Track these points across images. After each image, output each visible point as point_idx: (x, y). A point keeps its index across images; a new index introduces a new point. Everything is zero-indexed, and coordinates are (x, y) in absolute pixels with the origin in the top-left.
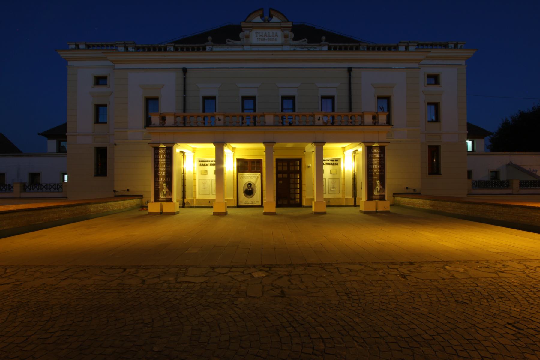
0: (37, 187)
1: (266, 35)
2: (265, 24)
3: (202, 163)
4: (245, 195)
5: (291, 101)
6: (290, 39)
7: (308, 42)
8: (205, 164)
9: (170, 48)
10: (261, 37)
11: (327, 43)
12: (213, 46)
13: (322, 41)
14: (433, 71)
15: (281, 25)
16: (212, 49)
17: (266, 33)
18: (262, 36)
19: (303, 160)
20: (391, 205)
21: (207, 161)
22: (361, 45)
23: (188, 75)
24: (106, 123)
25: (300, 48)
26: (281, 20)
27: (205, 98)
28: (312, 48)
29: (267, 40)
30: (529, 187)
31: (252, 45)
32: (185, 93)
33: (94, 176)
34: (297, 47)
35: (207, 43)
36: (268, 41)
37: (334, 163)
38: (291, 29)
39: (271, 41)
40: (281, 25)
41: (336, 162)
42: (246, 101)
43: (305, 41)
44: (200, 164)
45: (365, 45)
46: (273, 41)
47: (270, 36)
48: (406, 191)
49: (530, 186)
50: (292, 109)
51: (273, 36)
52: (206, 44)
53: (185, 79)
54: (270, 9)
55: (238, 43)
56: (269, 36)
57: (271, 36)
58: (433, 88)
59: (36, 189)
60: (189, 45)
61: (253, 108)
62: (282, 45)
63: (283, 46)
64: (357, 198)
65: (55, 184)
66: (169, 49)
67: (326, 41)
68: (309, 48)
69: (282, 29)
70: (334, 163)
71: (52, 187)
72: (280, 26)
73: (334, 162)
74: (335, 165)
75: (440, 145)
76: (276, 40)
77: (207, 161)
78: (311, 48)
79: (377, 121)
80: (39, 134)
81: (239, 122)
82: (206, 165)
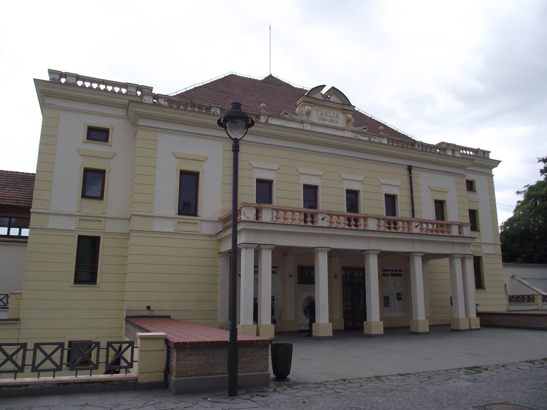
1: (327, 115)
4: (305, 315)
8: (386, 274)
9: (216, 110)
10: (322, 117)
14: (470, 177)
16: (267, 120)
18: (323, 116)
26: (343, 102)
28: (372, 138)
29: (327, 120)
30: (515, 302)
31: (312, 124)
34: (358, 134)
36: (329, 122)
39: (332, 122)
43: (365, 128)
46: (334, 123)
48: (147, 313)
49: (515, 301)
51: (334, 118)
57: (332, 117)
58: (471, 195)
62: (343, 130)
64: (238, 326)
66: (215, 110)
68: (369, 138)
73: (398, 272)
76: (337, 122)
78: (372, 137)
79: (450, 230)
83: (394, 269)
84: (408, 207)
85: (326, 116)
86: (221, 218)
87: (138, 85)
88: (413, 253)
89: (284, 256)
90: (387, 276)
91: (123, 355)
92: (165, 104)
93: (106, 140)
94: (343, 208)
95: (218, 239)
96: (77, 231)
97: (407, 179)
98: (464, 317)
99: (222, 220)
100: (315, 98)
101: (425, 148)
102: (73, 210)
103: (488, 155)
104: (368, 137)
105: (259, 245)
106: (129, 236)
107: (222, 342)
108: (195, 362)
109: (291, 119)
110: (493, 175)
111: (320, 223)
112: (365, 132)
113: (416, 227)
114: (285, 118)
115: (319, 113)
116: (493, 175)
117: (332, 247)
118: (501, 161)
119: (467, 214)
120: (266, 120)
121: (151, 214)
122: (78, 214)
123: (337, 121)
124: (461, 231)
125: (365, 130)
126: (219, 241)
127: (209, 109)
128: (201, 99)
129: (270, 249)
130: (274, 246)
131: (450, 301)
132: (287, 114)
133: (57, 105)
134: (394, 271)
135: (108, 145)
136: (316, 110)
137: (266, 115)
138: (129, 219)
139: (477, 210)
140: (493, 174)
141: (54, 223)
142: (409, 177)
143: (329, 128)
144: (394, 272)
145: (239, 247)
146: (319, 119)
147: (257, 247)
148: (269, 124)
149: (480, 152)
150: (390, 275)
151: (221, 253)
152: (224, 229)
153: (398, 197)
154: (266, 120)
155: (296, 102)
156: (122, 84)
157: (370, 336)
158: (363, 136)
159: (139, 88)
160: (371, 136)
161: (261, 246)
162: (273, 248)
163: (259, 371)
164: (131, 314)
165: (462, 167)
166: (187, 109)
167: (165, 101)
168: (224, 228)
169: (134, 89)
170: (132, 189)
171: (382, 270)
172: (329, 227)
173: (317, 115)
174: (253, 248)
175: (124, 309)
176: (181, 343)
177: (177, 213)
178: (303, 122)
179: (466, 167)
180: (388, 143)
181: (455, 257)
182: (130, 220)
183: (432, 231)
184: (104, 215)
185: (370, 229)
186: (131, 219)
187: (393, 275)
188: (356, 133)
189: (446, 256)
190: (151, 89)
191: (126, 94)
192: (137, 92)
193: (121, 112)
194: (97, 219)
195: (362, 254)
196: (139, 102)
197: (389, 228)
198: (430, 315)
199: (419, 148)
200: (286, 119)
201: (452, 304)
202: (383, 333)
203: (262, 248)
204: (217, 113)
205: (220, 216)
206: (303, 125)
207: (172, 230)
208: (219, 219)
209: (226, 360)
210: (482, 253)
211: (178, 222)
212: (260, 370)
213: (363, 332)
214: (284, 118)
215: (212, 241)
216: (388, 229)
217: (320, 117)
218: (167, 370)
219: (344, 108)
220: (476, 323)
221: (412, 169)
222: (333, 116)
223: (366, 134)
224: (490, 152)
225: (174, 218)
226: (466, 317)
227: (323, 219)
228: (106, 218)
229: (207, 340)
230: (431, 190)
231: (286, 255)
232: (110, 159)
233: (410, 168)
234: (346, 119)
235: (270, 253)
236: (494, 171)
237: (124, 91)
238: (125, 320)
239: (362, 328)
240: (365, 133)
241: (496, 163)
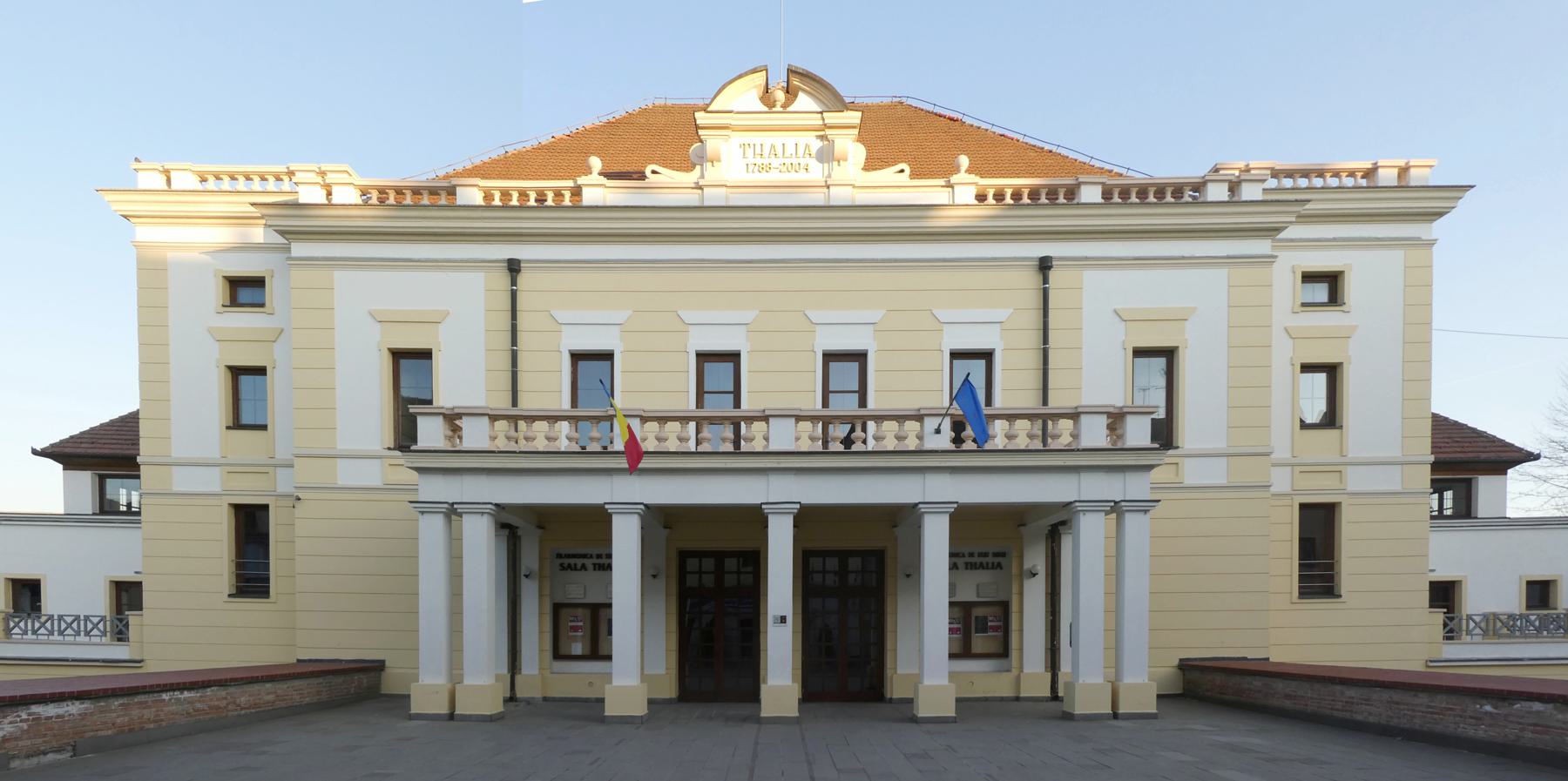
0: (22, 624)
3: (566, 561)
5: (854, 367)
7: (914, 175)
8: (575, 564)
11: (973, 176)
13: (957, 170)
19: (549, 654)
20: (1159, 696)
21: (584, 556)
24: (264, 427)
27: (577, 357)
32: (514, 342)
33: (230, 596)
35: (584, 177)
37: (987, 564)
38: (856, 131)
41: (997, 560)
42: (708, 366)
43: (902, 171)
44: (561, 565)
52: (581, 180)
53: (514, 295)
54: (792, 71)
59: (42, 631)
61: (731, 389)
65: (77, 618)
67: (969, 171)
70: (987, 564)
71: (69, 625)
73: (990, 559)
74: (993, 568)
75: (1340, 503)
77: (584, 556)
80: (35, 452)
81: (687, 440)
82: (579, 567)
90: (581, 570)
96: (1295, 495)
97: (1034, 300)
101: (1191, 193)
102: (214, 454)
105: (1116, 503)
115: (749, 152)
122: (223, 461)
127: (1071, 193)
133: (1424, 238)
134: (976, 555)
135: (1343, 311)
141: (182, 480)
144: (976, 560)
145: (456, 509)
148: (460, 206)
150: (590, 567)
161: (921, 506)
165: (1271, 231)
166: (1057, 202)
179: (1279, 230)
180: (576, 198)
194: (1336, 469)
195: (754, 518)
202: (797, 714)
203: (923, 510)
207: (377, 483)
210: (1344, 494)
221: (1050, 268)
225: (380, 457)
228: (276, 466)
231: (1023, 525)
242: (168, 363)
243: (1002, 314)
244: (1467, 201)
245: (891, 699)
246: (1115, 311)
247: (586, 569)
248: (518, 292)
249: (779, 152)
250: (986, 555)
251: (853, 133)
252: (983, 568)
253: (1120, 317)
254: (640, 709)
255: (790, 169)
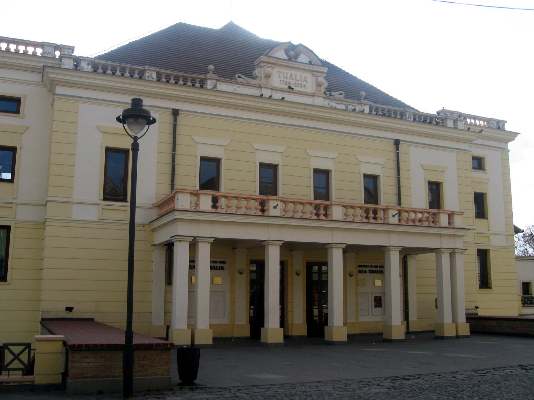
2: (290, 62)
6: (323, 88)
12: (218, 80)
14: (478, 152)
15: (313, 68)
17: (291, 75)
21: (365, 266)
22: (407, 111)
23: (179, 118)
25: (335, 103)
32: (174, 149)
34: (332, 101)
37: (362, 270)
40: (313, 68)
41: (221, 265)
43: (341, 94)
45: (412, 112)
47: (297, 79)
50: (324, 188)
51: (301, 81)
55: (254, 82)
56: (296, 80)
57: (298, 81)
58: (478, 174)
60: (181, 74)
62: (313, 96)
63: (315, 97)
68: (346, 105)
69: (314, 73)
72: (312, 69)
73: (378, 269)
76: (305, 86)
77: (365, 266)
78: (349, 104)
83: (373, 265)
84: (393, 190)
85: (291, 79)
86: (155, 204)
87: (57, 44)
88: (331, 245)
89: (233, 249)
90: (364, 273)
91: (19, 357)
92: (88, 69)
93: (17, 112)
94: (308, 194)
95: (151, 229)
97: (393, 156)
98: (451, 321)
99: (156, 206)
100: (277, 58)
103: (503, 125)
104: (345, 105)
105: (195, 237)
106: (45, 225)
107: (120, 345)
108: (91, 365)
109: (246, 84)
110: (509, 150)
111: (272, 212)
112: (341, 99)
113: (393, 216)
114: (238, 82)
115: (282, 76)
116: (509, 150)
117: (404, 246)
118: (519, 133)
119: (472, 199)
120: (214, 85)
121: (70, 200)
123: (305, 85)
124: (451, 221)
125: (341, 96)
126: (153, 230)
128: (210, 55)
129: (209, 243)
130: (346, 245)
131: (435, 303)
132: (241, 78)
135: (485, 173)
136: (279, 72)
137: (214, 79)
138: (45, 205)
139: (486, 194)
140: (509, 149)
142: (396, 153)
143: (293, 94)
145: (198, 240)
146: (282, 82)
147: (192, 240)
149: (492, 122)
150: (368, 271)
151: (155, 245)
152: (160, 217)
153: (381, 177)
154: (214, 85)
155: (253, 62)
156: (37, 43)
157: (331, 344)
158: (337, 104)
159: (57, 47)
160: (349, 103)
162: (212, 241)
163: (160, 374)
164: (47, 316)
167: (88, 65)
168: (159, 215)
169: (52, 49)
170: (48, 170)
171: (357, 266)
172: (283, 217)
173: (280, 77)
174: (279, 245)
175: (40, 311)
176: (76, 346)
177: (102, 199)
178: (261, 87)
181: (441, 252)
182: (46, 206)
183: (414, 221)
184: (14, 201)
185: (334, 218)
186: (47, 205)
187: (371, 272)
188: (329, 100)
189: (431, 250)
190: (72, 49)
191: (42, 56)
192: (55, 52)
193: (36, 77)
196: (58, 66)
197: (367, 218)
198: (416, 320)
199: (411, 118)
200: (239, 83)
201: (437, 307)
202: (404, 338)
204: (152, 77)
205: (154, 201)
206: (261, 90)
208: (154, 205)
209: (122, 364)
211: (103, 209)
212: (161, 374)
213: (324, 339)
214: (237, 83)
215: (145, 231)
216: (315, 216)
217: (283, 81)
218: (65, 375)
219: (315, 69)
220: (465, 329)
222: (300, 79)
223: (342, 101)
224: (506, 122)
226: (453, 322)
227: (275, 207)
228: (16, 204)
229: (105, 343)
230: (425, 169)
232: (22, 133)
233: (397, 143)
234: (316, 83)
235: (341, 252)
236: (511, 145)
237: (39, 51)
238: (40, 323)
239: (322, 335)
240: (341, 100)
241: (513, 135)
242: (410, 171)
243: (382, 161)
244: (518, 136)
245: (292, 336)
246: (421, 165)
247: (366, 273)
248: (177, 125)
249: (294, 78)
250: (376, 267)
251: (324, 75)
252: (215, 269)
253: (423, 168)
254: (210, 342)
255: (298, 85)
